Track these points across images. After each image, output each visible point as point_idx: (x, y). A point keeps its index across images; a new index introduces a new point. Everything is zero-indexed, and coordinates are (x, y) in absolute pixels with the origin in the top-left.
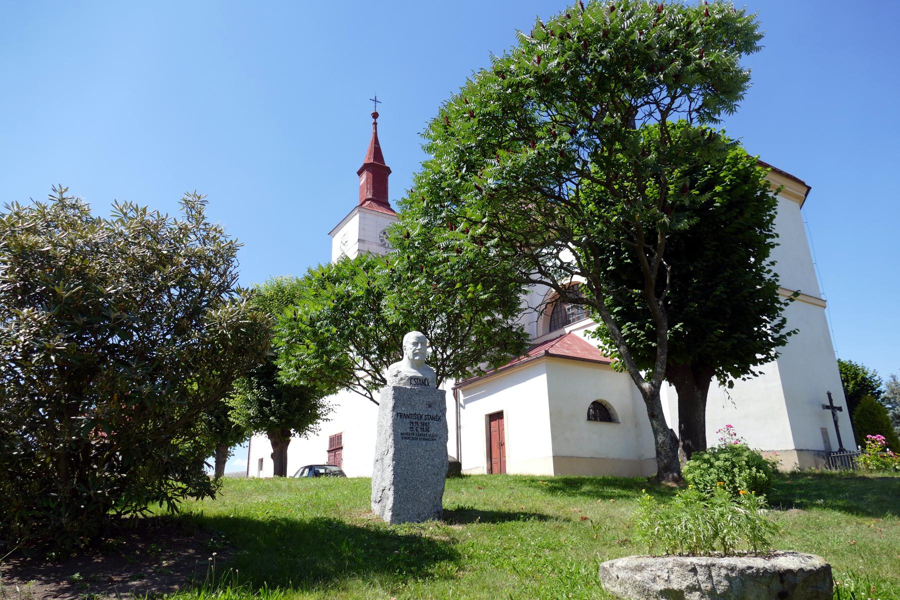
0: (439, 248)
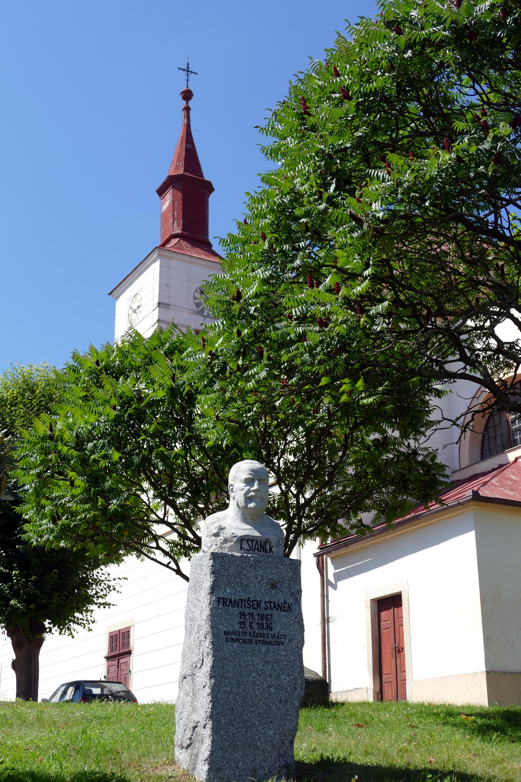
0: (290, 317)
